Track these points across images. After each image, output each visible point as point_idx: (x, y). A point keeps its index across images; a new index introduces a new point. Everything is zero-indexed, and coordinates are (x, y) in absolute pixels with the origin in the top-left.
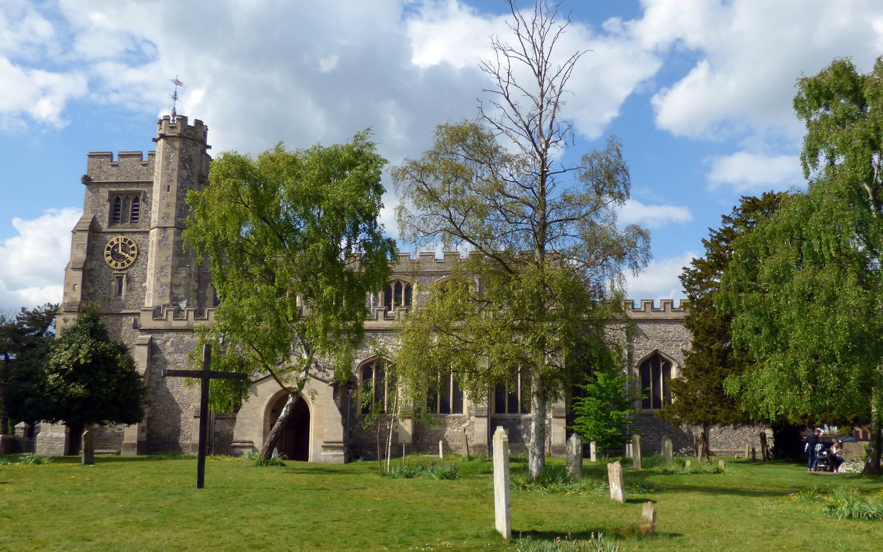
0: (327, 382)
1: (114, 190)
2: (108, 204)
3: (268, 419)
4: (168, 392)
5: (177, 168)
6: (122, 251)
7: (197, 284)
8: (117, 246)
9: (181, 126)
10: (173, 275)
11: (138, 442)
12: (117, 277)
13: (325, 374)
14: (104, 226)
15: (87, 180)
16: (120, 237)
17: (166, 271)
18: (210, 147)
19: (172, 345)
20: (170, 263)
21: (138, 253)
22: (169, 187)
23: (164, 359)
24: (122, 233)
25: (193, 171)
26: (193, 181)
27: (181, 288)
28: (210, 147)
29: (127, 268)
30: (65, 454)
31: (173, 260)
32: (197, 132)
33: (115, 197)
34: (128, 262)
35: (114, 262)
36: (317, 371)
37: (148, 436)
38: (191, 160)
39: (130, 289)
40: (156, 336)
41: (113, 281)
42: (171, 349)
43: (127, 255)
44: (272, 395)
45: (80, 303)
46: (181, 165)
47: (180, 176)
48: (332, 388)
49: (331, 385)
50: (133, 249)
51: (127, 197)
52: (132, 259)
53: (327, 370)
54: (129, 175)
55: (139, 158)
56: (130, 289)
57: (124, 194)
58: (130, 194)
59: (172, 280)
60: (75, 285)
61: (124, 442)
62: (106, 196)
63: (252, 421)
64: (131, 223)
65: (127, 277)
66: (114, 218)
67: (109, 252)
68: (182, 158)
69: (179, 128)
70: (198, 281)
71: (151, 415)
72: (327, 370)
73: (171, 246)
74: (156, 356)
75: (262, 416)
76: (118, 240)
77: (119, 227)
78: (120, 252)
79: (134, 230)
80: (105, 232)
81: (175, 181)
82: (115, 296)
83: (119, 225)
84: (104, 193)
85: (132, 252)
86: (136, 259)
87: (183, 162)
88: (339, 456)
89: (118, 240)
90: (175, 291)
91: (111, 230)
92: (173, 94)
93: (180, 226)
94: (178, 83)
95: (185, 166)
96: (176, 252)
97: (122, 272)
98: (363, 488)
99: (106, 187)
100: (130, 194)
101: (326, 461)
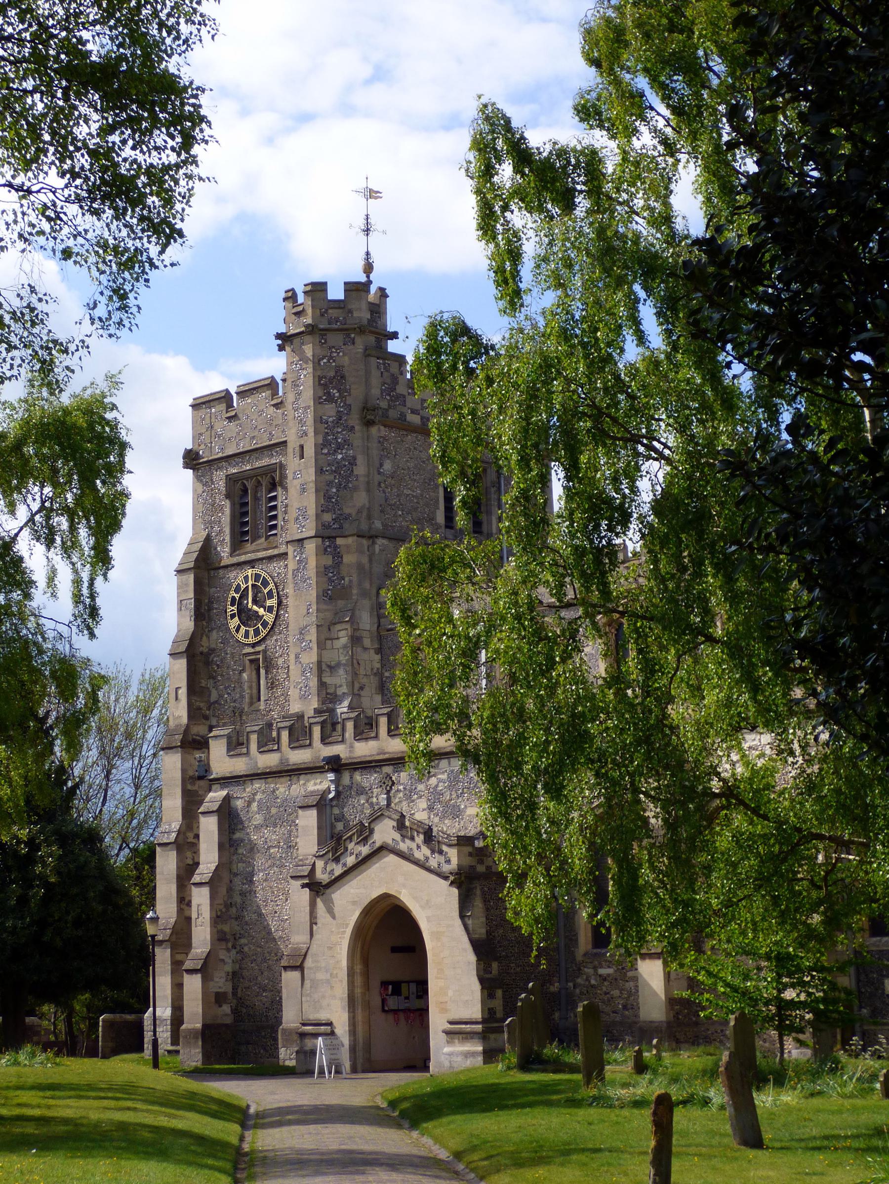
0: (446, 878)
1: (235, 471)
2: (227, 504)
3: (358, 968)
4: (260, 915)
5: (312, 403)
6: (255, 602)
7: (378, 657)
8: (244, 595)
9: (313, 307)
10: (321, 646)
11: (205, 1026)
12: (251, 661)
13: (442, 859)
14: (224, 551)
15: (191, 459)
16: (250, 572)
17: (307, 638)
18: (394, 335)
19: (260, 808)
20: (314, 619)
21: (280, 603)
22: (302, 447)
23: (250, 840)
24: (251, 563)
25: (349, 401)
26: (351, 423)
27: (341, 671)
28: (394, 335)
29: (264, 639)
30: (203, 1064)
31: (318, 610)
32: (350, 311)
33: (239, 485)
34: (265, 624)
35: (243, 629)
36: (428, 852)
37: (235, 1011)
38: (343, 377)
39: (272, 686)
40: (236, 791)
41: (243, 670)
42: (258, 819)
43: (261, 611)
44: (357, 914)
45: (188, 726)
46: (320, 393)
47: (319, 420)
48: (455, 891)
49: (452, 883)
50: (270, 595)
51: (259, 482)
52: (270, 618)
53: (445, 848)
54: (256, 433)
55: (269, 392)
56: (272, 686)
57: (252, 478)
58: (261, 475)
59: (320, 655)
60: (177, 689)
61: (183, 1027)
62: (221, 485)
63: (328, 975)
64: (267, 537)
65: (265, 658)
66: (240, 537)
67: (235, 608)
68: (320, 378)
69: (309, 311)
70: (379, 651)
71: (237, 966)
72: (445, 848)
73: (313, 581)
74: (238, 835)
75: (344, 963)
76: (246, 578)
77: (252, 551)
78: (250, 604)
79: (270, 552)
80: (226, 567)
81: (311, 433)
82: (251, 704)
83: (249, 547)
84: (219, 478)
85: (269, 603)
86: (277, 616)
87: (325, 386)
88: (473, 1054)
89: (246, 578)
90: (327, 680)
91: (235, 560)
92: (361, 223)
93: (327, 533)
94: (372, 194)
95: (329, 393)
96: (325, 592)
97: (258, 649)
98: (822, 1174)
99: (220, 468)
100: (247, 479)
101: (451, 1067)
